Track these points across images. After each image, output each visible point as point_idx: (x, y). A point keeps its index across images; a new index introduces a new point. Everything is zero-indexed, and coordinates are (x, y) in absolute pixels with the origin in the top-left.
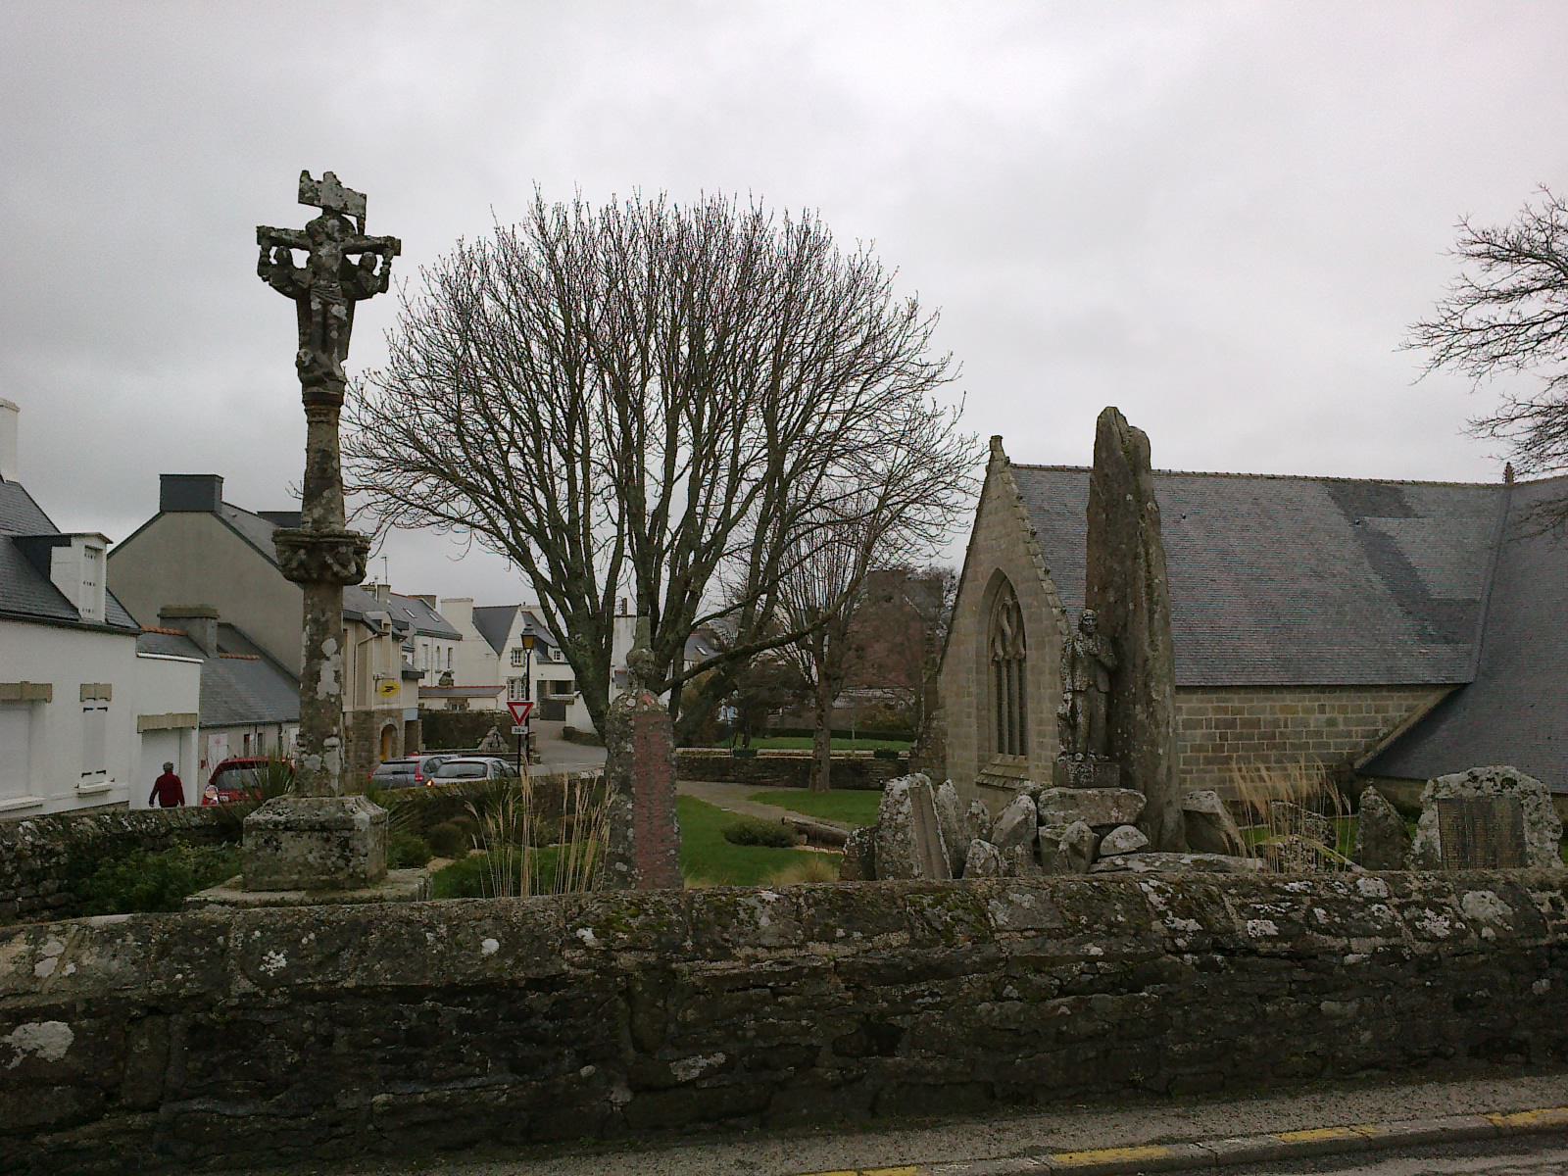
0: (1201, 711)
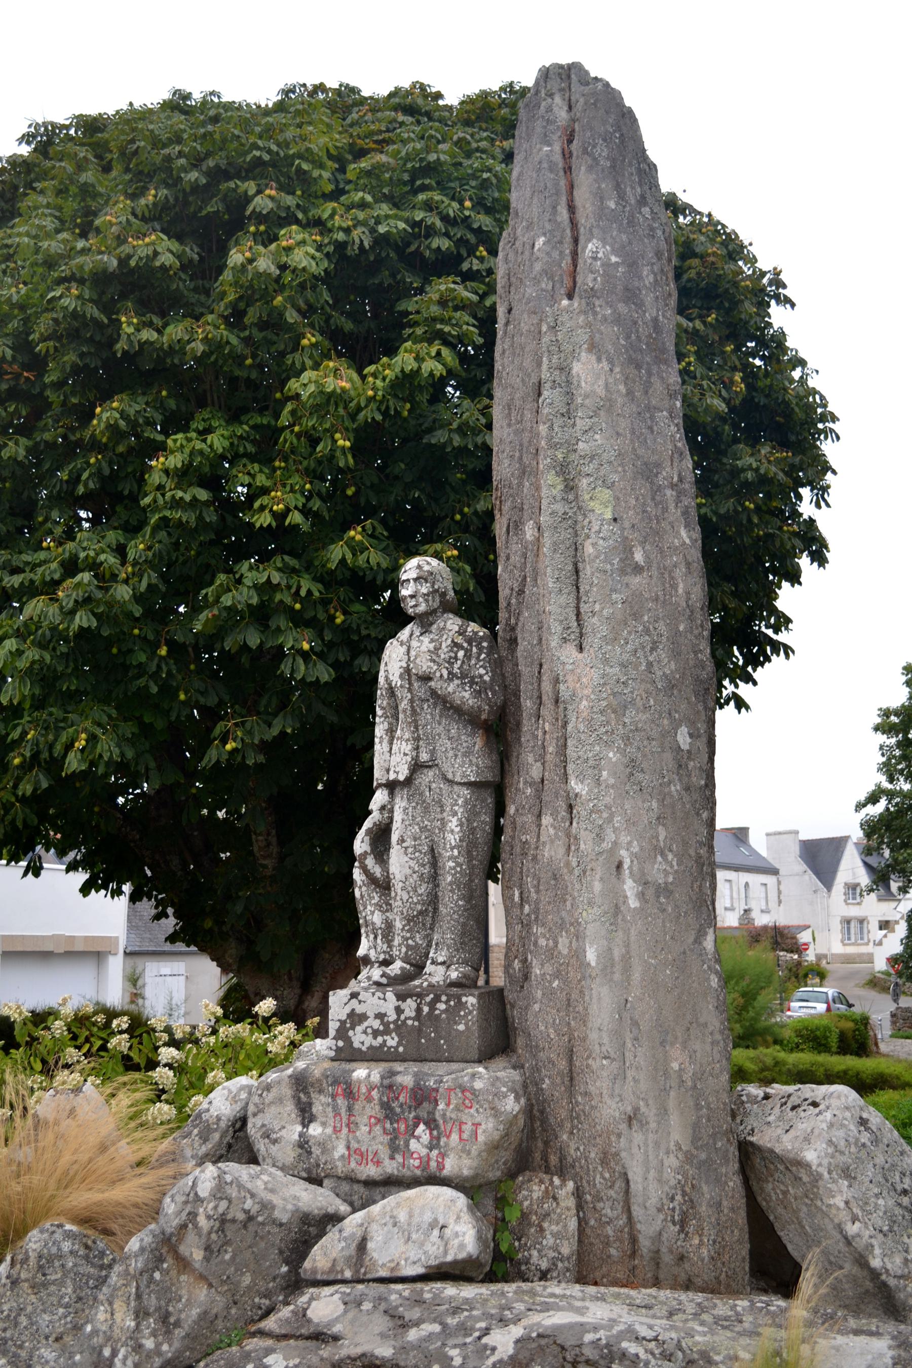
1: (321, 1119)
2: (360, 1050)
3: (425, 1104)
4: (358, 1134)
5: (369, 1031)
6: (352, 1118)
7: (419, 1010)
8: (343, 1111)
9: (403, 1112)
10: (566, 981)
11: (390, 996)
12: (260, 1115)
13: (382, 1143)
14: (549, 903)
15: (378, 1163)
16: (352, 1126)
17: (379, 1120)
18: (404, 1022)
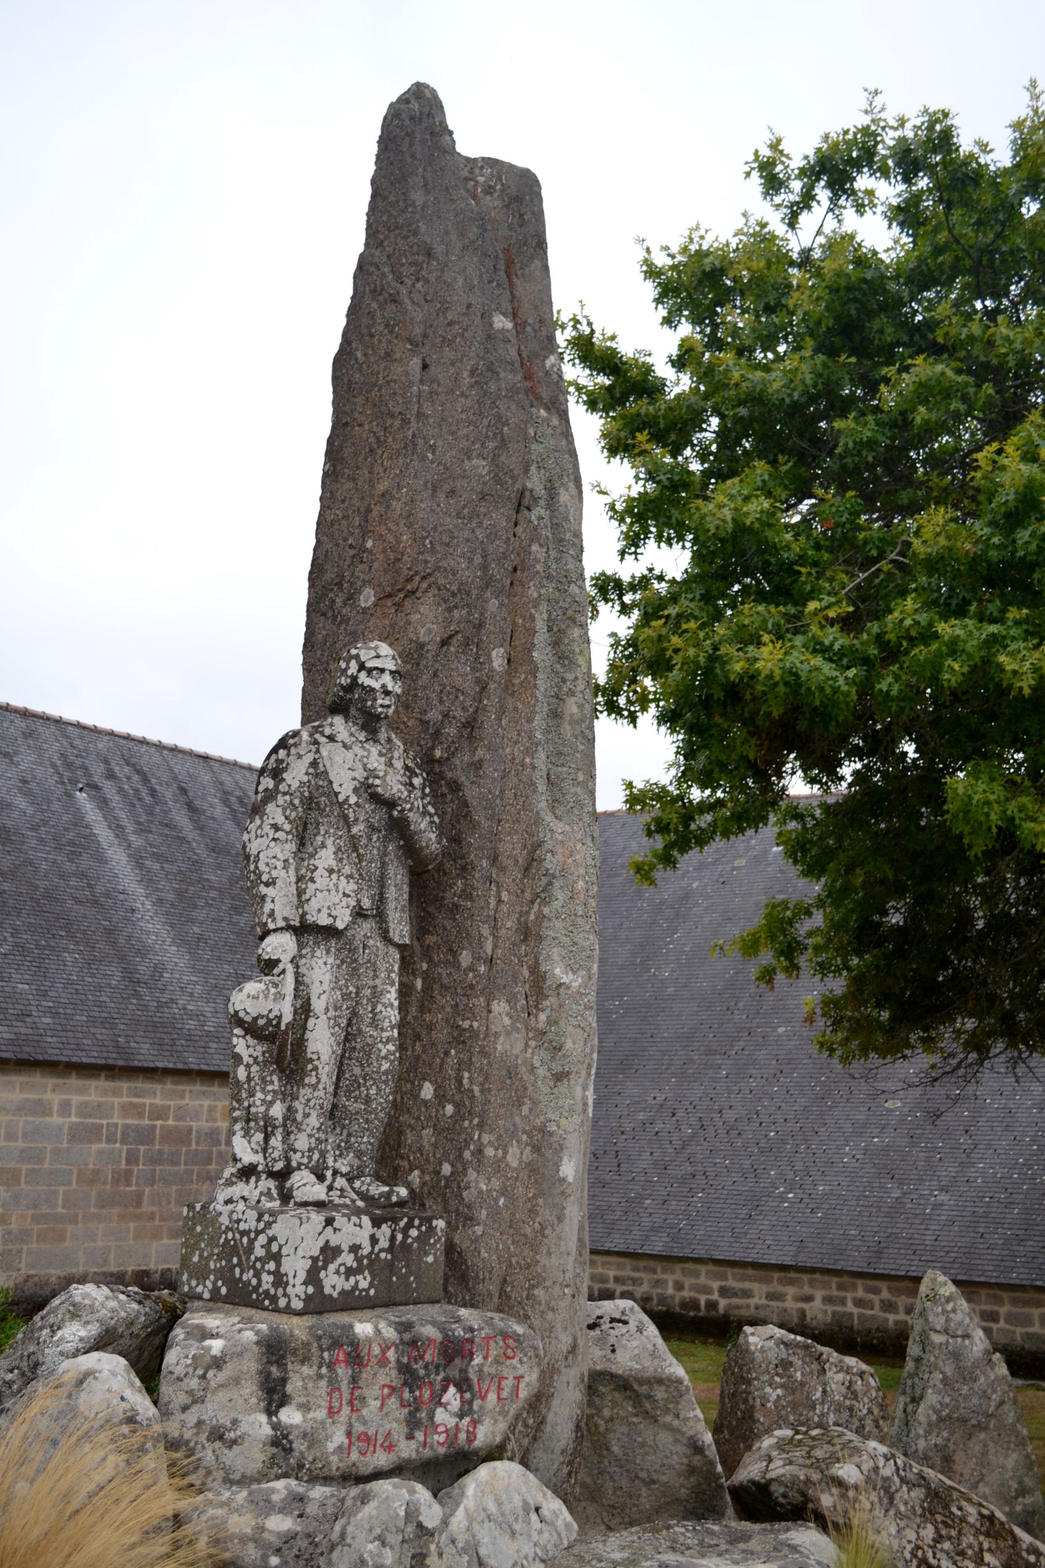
0: (100, 1109)
1: (299, 1399)
2: (331, 1296)
3: (457, 1361)
4: (364, 1412)
5: (342, 1269)
6: (357, 1393)
7: (393, 1238)
8: (345, 1386)
9: (428, 1375)
10: (512, 1199)
11: (366, 1220)
12: (195, 1409)
13: (396, 1420)
14: (502, 1106)
15: (390, 1448)
16: (356, 1402)
17: (393, 1389)
18: (377, 1255)
